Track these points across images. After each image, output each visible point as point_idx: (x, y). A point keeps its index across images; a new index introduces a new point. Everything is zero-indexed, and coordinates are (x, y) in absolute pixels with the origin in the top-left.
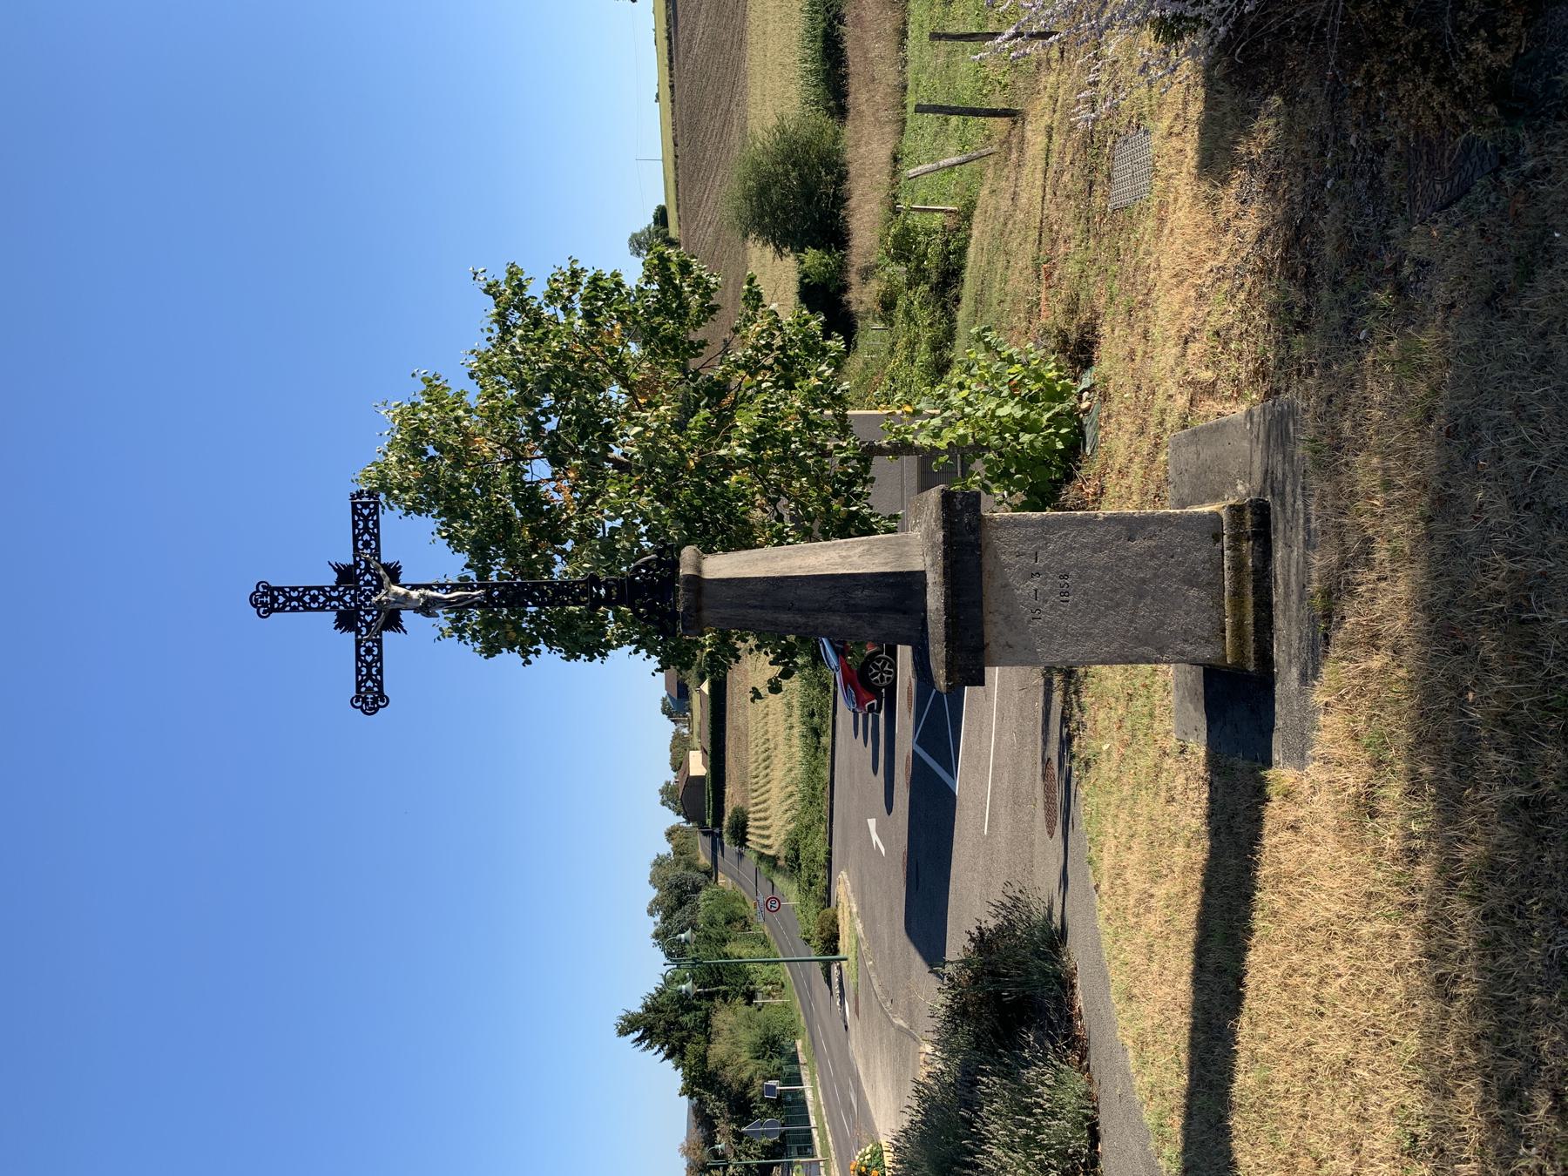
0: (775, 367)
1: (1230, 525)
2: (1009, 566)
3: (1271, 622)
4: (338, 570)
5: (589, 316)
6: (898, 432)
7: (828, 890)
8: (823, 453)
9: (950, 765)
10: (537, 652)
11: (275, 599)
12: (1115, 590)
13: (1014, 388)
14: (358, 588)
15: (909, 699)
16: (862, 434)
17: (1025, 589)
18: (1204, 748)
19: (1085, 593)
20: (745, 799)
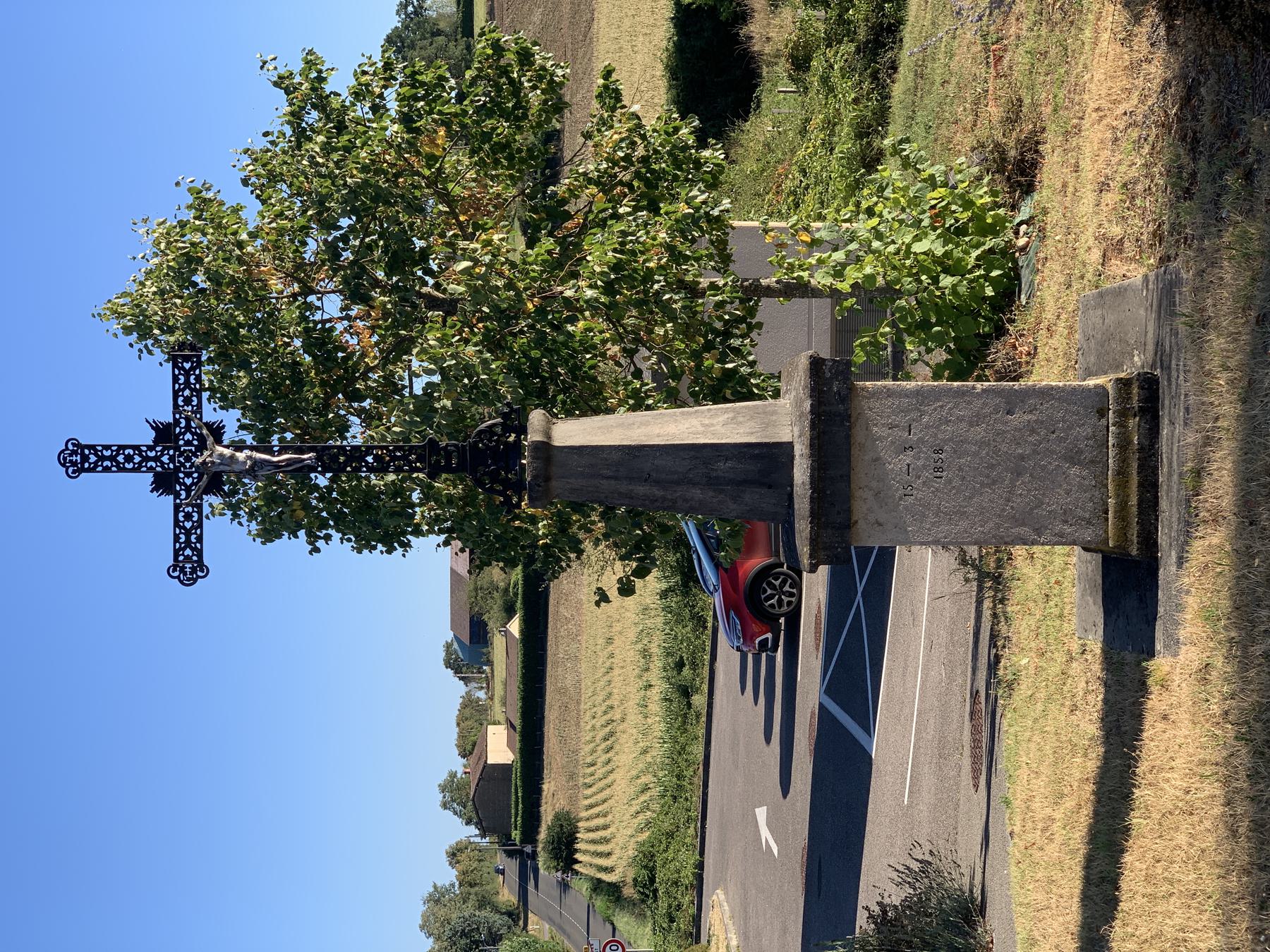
0: (636, 184)
1: (1116, 400)
2: (880, 438)
3: (1157, 504)
4: (155, 428)
5: (406, 120)
6: (791, 268)
7: (697, 920)
8: (693, 291)
9: (866, 720)
10: (328, 538)
11: (85, 458)
12: (992, 467)
13: (939, 215)
14: (177, 448)
15: (817, 631)
16: (743, 268)
17: (897, 464)
18: (1100, 645)
19: (960, 469)
20: (573, 800)
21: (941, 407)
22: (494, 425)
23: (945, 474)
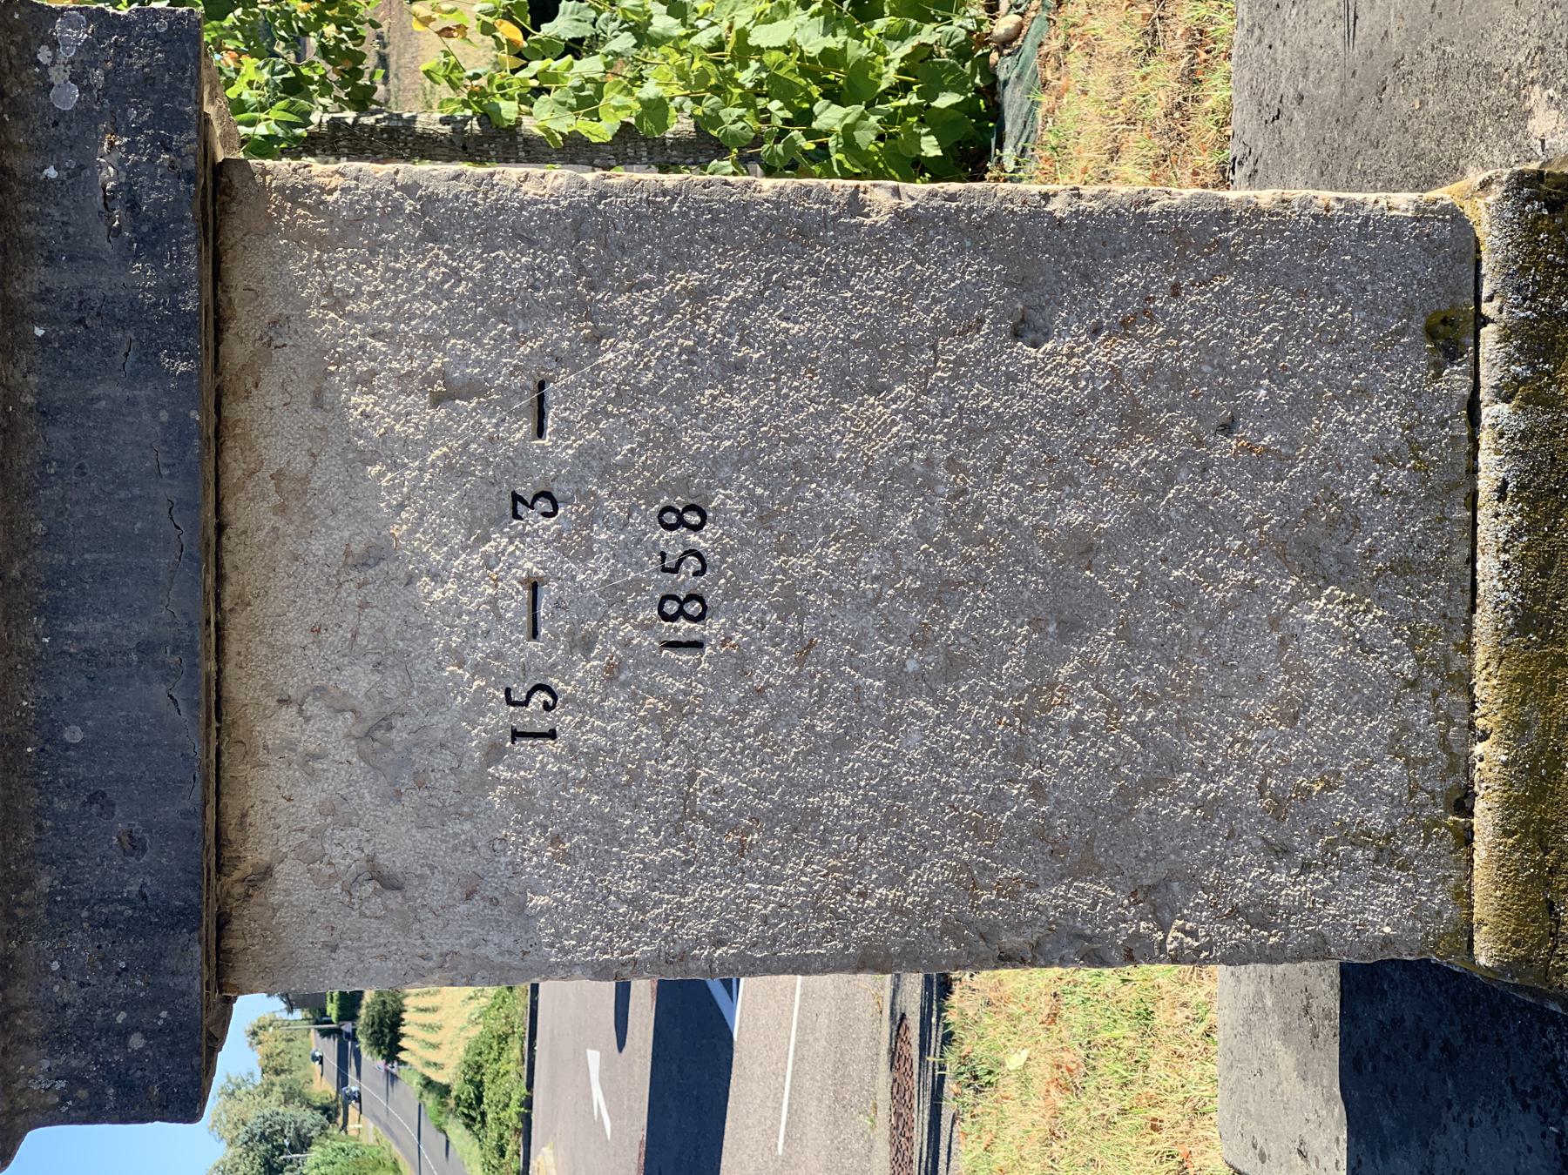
2: (388, 451)
12: (942, 592)
19: (790, 605)
21: (698, 295)
23: (713, 627)
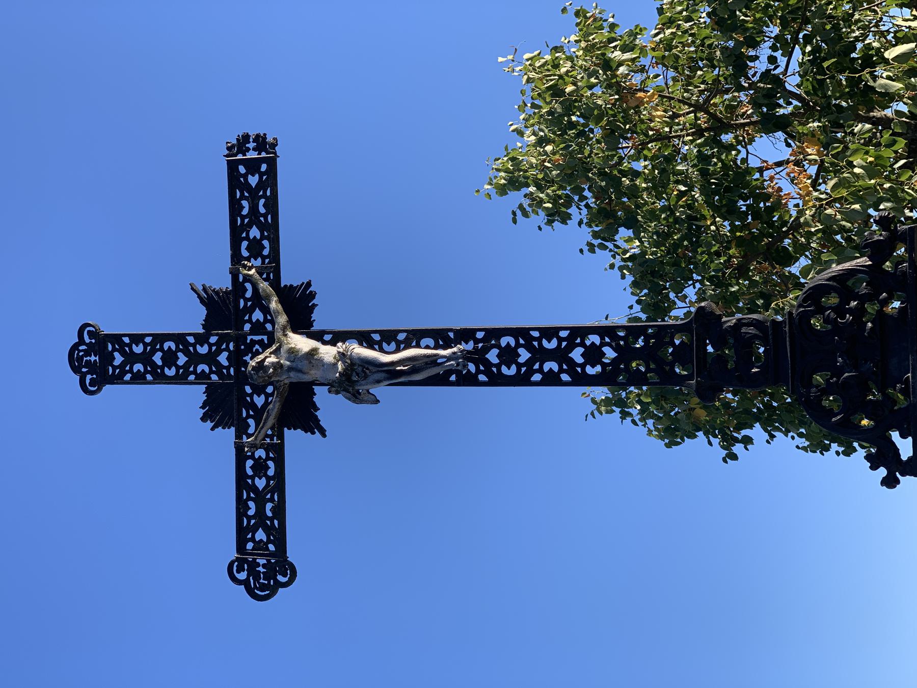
10: (747, 441)
22: (851, 272)
